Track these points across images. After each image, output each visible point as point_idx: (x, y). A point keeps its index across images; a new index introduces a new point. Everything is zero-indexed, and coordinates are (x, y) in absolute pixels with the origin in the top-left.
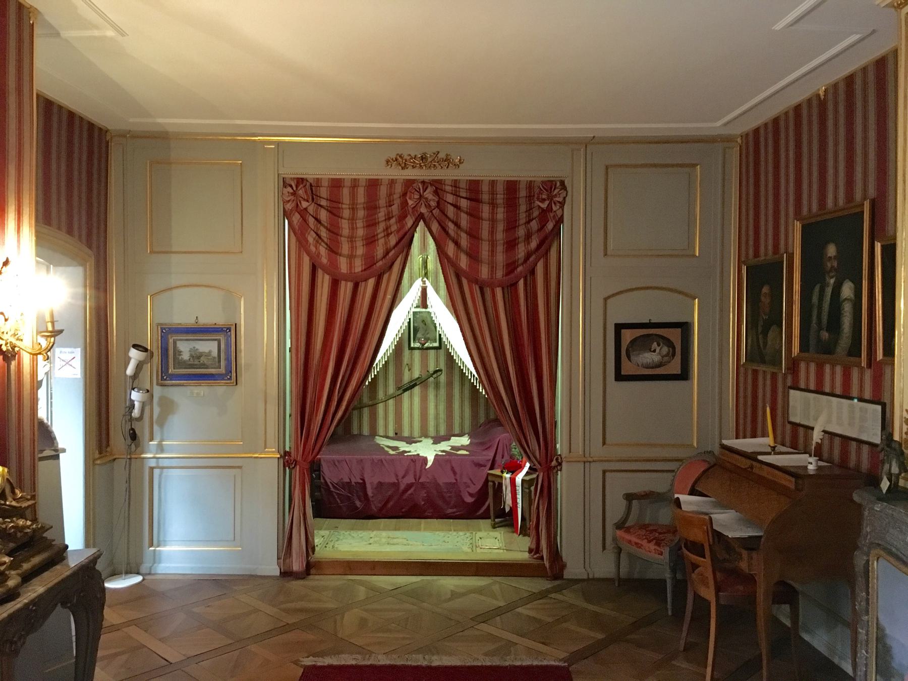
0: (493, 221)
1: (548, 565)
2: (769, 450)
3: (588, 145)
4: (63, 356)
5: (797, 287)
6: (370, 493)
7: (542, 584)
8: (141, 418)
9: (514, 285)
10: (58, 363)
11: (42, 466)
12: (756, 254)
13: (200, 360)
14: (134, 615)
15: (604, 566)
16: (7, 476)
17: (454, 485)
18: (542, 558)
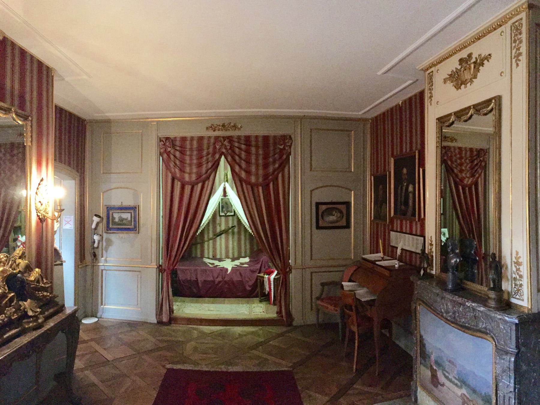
0: (257, 155)
1: (285, 319)
2: (381, 259)
3: (302, 119)
4: (66, 219)
5: (392, 186)
6: (200, 285)
7: (284, 329)
8: (98, 247)
9: (268, 185)
10: (64, 223)
11: (56, 268)
12: (377, 172)
13: (121, 221)
14: (93, 336)
15: (311, 319)
16: (40, 273)
17: (241, 282)
18: (282, 316)
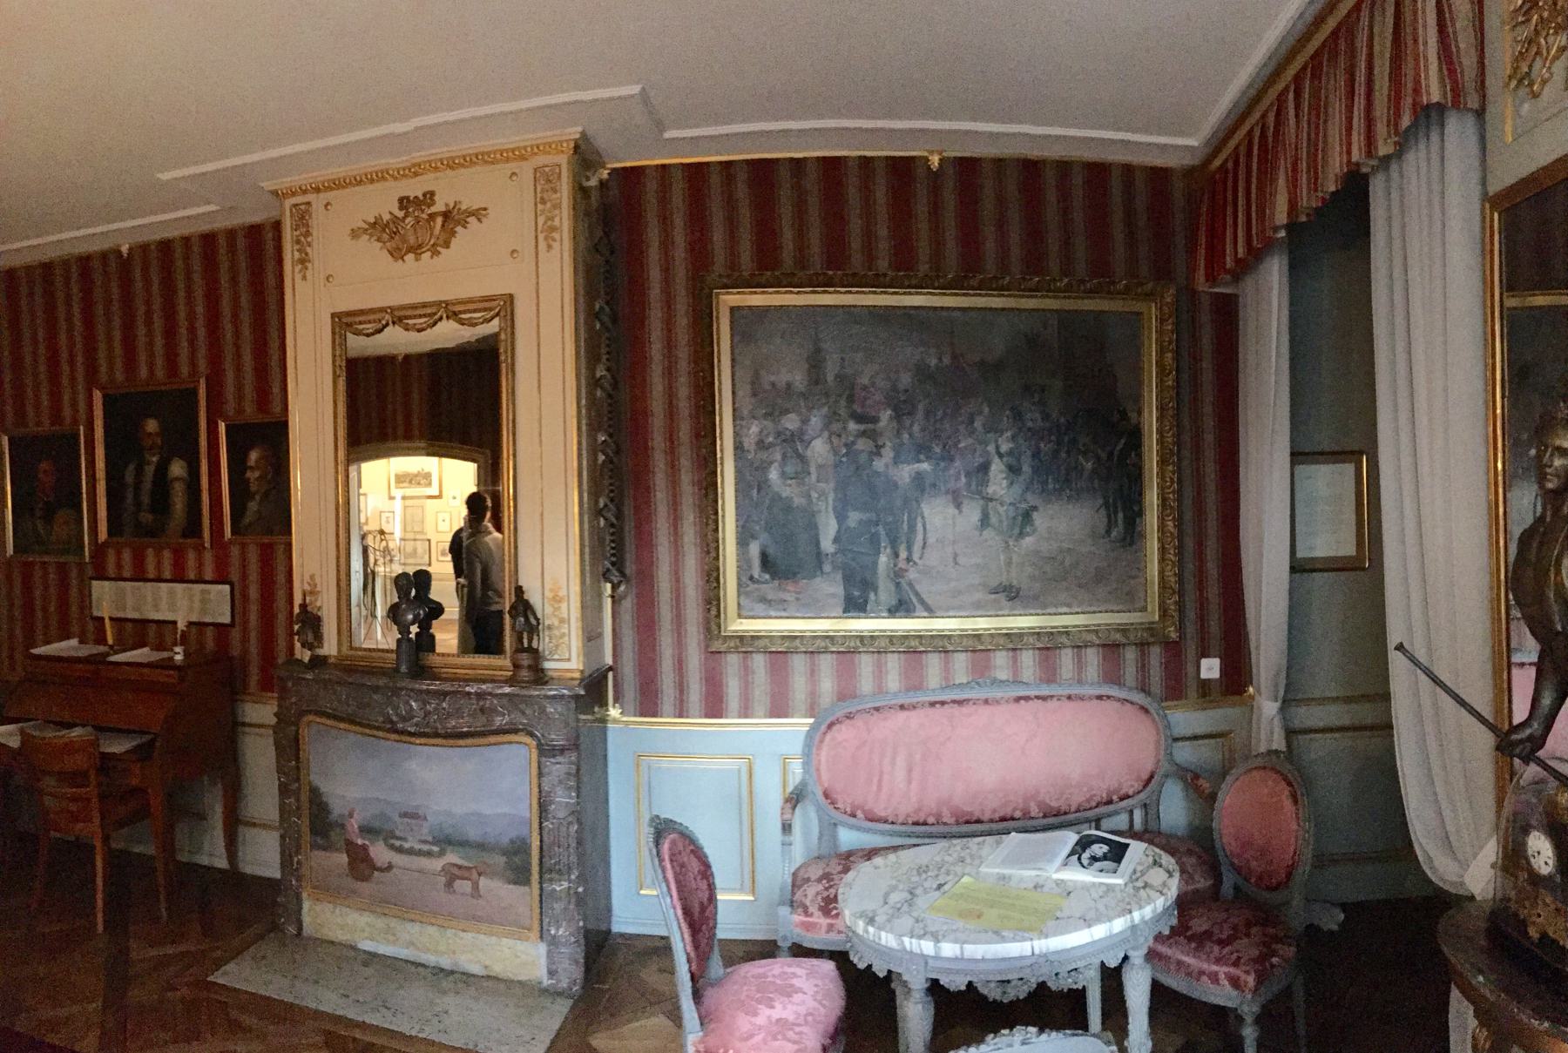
5: (100, 464)
